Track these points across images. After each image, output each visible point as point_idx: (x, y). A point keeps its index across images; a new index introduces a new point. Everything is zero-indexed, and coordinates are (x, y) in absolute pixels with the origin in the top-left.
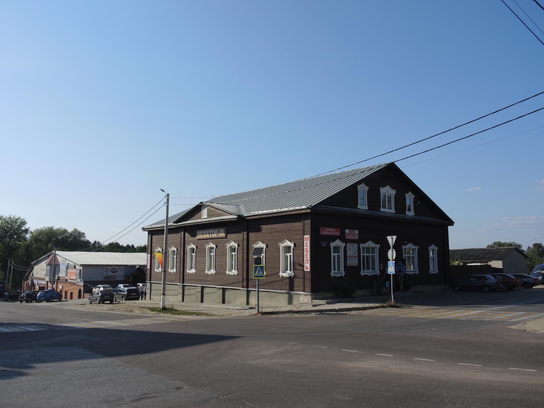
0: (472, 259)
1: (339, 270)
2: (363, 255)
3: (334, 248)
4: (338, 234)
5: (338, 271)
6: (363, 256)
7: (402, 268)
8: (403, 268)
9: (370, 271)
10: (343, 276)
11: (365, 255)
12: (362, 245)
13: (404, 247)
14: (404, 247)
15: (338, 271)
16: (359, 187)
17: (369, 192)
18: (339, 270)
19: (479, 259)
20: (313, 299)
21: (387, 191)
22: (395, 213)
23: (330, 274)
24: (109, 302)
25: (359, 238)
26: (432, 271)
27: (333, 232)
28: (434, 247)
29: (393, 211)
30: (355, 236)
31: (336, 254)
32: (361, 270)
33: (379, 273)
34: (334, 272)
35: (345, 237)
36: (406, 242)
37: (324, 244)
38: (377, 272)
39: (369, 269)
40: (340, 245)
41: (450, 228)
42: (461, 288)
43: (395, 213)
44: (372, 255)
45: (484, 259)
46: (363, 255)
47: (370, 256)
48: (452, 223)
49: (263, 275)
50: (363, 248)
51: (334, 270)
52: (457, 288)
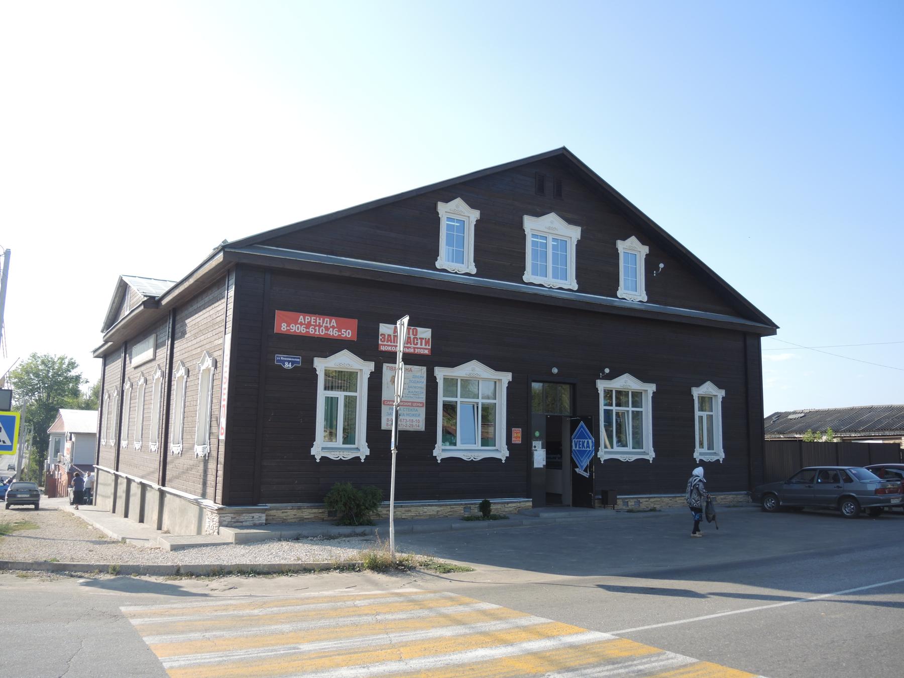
0: (863, 431)
1: (710, 447)
2: (605, 410)
3: (702, 399)
4: (348, 334)
5: (482, 446)
6: (608, 413)
7: (586, 441)
8: (588, 441)
9: (629, 449)
10: (651, 460)
11: (614, 408)
12: (441, 373)
13: (602, 385)
14: (602, 385)
15: (482, 446)
16: (443, 209)
17: (480, 228)
18: (710, 447)
19: (878, 430)
20: (225, 523)
21: (549, 228)
22: (575, 291)
23: (693, 455)
24: (32, 506)
25: (432, 350)
26: (701, 454)
27: (327, 328)
28: (712, 391)
29: (572, 283)
30: (419, 346)
31: (704, 414)
32: (694, 447)
33: (507, 453)
34: (443, 448)
35: (377, 345)
36: (607, 371)
37: (289, 362)
38: (648, 454)
39: (625, 445)
40: (715, 393)
41: (766, 342)
42: (781, 503)
43: (575, 291)
44: (633, 412)
45: (891, 430)
46: (605, 410)
47: (628, 411)
48: (770, 328)
49: (8, 443)
50: (608, 393)
51: (701, 444)
52: (769, 504)
